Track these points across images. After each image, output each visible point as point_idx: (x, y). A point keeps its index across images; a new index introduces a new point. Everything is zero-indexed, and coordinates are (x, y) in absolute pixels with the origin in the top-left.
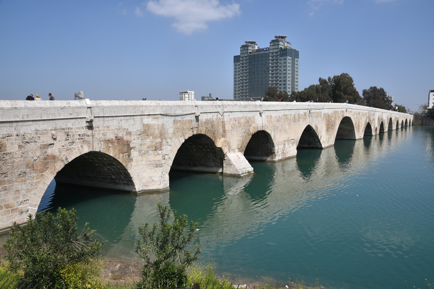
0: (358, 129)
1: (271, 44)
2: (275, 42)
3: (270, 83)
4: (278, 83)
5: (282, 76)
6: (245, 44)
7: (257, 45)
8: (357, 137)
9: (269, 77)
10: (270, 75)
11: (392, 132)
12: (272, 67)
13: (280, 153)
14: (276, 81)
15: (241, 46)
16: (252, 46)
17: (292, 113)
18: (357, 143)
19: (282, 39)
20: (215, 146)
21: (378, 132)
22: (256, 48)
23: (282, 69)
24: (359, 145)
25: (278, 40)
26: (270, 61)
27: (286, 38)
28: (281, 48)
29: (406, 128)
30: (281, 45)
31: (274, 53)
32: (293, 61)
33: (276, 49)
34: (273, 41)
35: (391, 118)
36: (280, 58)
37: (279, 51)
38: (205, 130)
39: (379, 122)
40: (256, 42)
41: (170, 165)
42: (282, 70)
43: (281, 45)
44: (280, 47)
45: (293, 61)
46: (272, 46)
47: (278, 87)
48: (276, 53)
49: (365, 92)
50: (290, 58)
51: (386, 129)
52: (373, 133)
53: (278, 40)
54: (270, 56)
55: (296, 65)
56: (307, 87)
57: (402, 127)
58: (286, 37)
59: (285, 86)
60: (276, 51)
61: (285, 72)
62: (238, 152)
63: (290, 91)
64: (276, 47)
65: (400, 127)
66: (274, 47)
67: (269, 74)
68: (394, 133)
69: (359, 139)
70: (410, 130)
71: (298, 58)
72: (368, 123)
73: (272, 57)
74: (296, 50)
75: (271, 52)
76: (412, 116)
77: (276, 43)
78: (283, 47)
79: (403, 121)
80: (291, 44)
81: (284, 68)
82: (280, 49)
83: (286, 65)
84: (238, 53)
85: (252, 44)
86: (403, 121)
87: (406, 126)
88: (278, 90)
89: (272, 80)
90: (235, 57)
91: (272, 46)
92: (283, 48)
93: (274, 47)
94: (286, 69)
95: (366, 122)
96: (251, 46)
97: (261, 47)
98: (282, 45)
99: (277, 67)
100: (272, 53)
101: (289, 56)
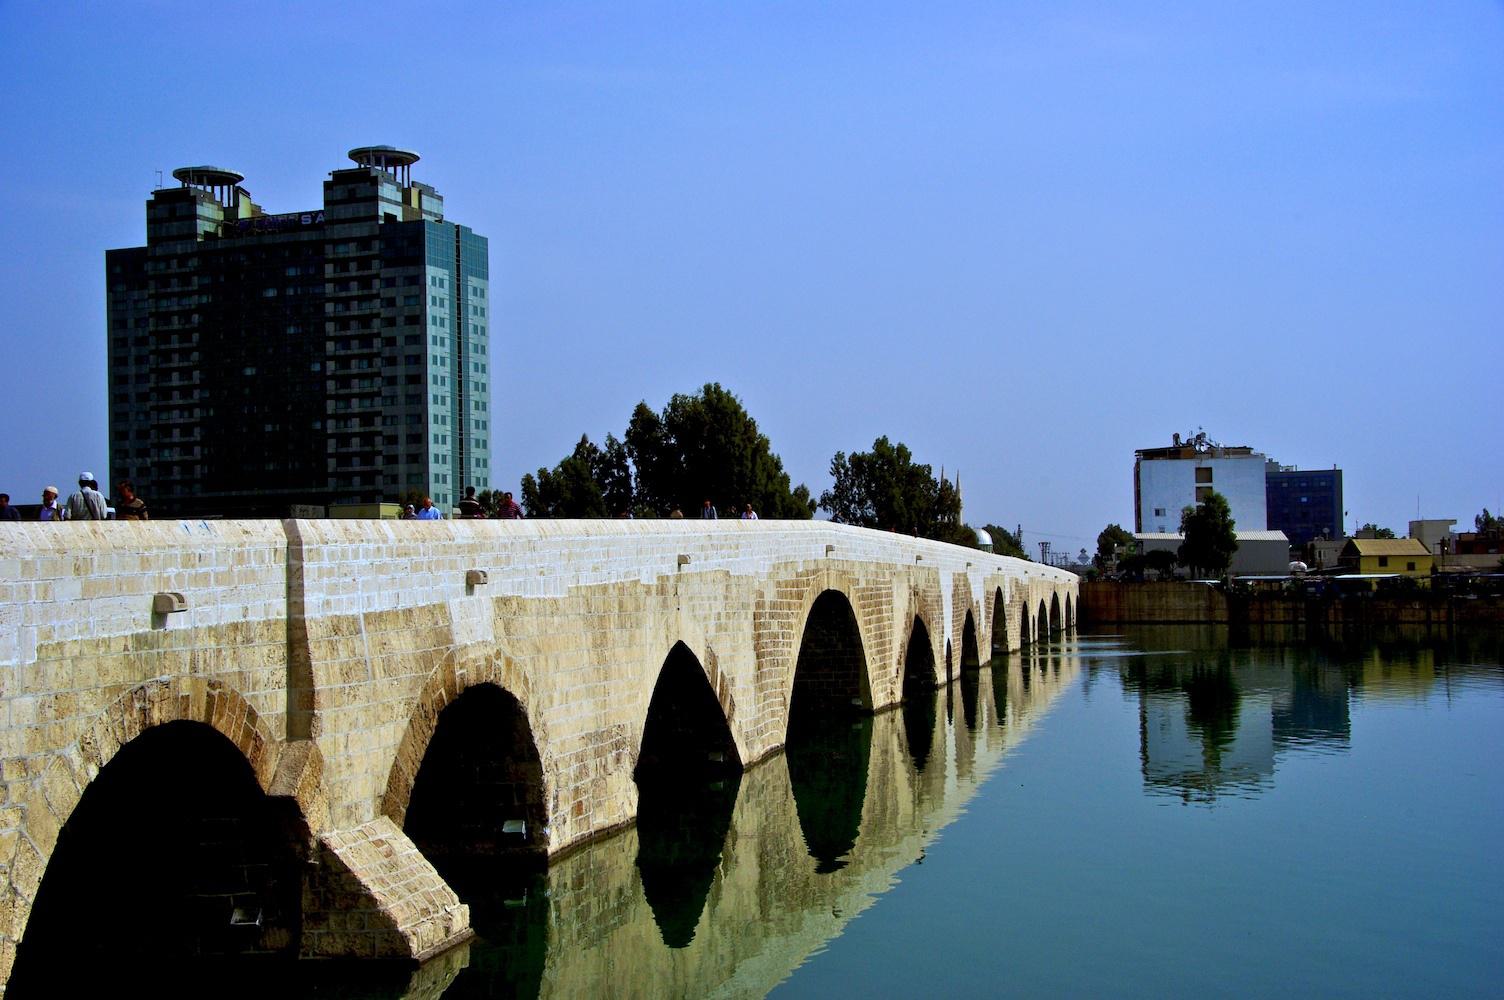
0: (879, 652)
6: (177, 184)
8: (879, 699)
9: (323, 377)
11: (1008, 661)
13: (566, 808)
16: (218, 198)
17: (610, 579)
18: (880, 723)
19: (391, 170)
20: (506, 820)
21: (956, 671)
22: (244, 213)
24: (887, 735)
25: (373, 174)
26: (329, 288)
27: (411, 165)
28: (390, 218)
29: (1056, 639)
30: (388, 201)
34: (340, 177)
35: (999, 594)
36: (387, 273)
37: (377, 232)
38: (205, 698)
39: (956, 615)
40: (241, 179)
41: (15, 938)
42: (400, 340)
43: (388, 201)
49: (915, 464)
51: (985, 654)
52: (941, 677)
53: (373, 174)
55: (475, 313)
56: (628, 425)
57: (1042, 638)
58: (417, 158)
61: (412, 350)
62: (376, 817)
63: (444, 457)
64: (362, 210)
65: (1034, 636)
68: (1014, 665)
69: (883, 710)
70: (1071, 650)
71: (485, 276)
72: (917, 617)
75: (179, 252)
76: (1075, 578)
77: (362, 190)
79: (1042, 604)
80: (440, 198)
81: (409, 330)
82: (381, 222)
84: (137, 237)
85: (399, 169)
86: (1042, 604)
87: (1056, 632)
90: (116, 259)
92: (400, 219)
93: (344, 212)
94: (418, 333)
95: (908, 615)
96: (212, 200)
97: (271, 210)
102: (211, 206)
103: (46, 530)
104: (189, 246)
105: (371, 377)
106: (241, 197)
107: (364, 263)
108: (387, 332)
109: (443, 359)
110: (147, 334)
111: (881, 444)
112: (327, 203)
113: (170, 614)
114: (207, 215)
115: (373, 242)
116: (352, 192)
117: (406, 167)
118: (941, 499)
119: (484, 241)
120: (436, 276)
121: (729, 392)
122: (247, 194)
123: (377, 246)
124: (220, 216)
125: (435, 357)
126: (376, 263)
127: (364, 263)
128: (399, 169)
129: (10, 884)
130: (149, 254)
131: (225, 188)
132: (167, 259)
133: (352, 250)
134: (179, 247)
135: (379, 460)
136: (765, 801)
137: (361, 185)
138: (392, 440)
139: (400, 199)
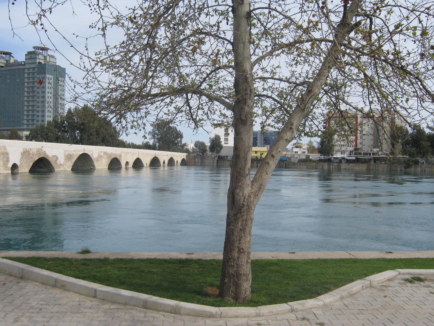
1: (27, 57)
2: (31, 55)
3: (25, 109)
4: (35, 76)
5: (40, 99)
6: (33, 50)
7: (13, 57)
10: (26, 99)
12: (28, 83)
14: (33, 111)
15: (27, 53)
22: (12, 61)
23: (40, 109)
28: (40, 63)
31: (31, 70)
32: (57, 80)
33: (32, 63)
34: (29, 53)
37: (36, 66)
44: (37, 62)
45: (57, 80)
46: (28, 59)
47: (35, 110)
48: (33, 68)
50: (52, 77)
54: (26, 73)
59: (43, 90)
60: (32, 66)
64: (33, 61)
66: (30, 61)
67: (23, 115)
73: (29, 74)
74: (61, 67)
77: (33, 56)
78: (43, 62)
80: (56, 59)
83: (44, 91)
85: (7, 56)
88: (35, 119)
89: (28, 104)
91: (28, 59)
92: (43, 63)
93: (30, 61)
98: (40, 59)
99: (34, 98)
100: (29, 69)
101: (49, 74)
105: (34, 101)
106: (11, 58)
107: (33, 74)
112: (26, 59)
113: (375, 33)
120: (50, 78)
121: (126, 141)
122: (13, 57)
123: (36, 69)
124: (5, 62)
126: (36, 74)
127: (33, 74)
133: (31, 71)
135: (35, 121)
136: (423, 94)
138: (38, 116)
139: (43, 59)
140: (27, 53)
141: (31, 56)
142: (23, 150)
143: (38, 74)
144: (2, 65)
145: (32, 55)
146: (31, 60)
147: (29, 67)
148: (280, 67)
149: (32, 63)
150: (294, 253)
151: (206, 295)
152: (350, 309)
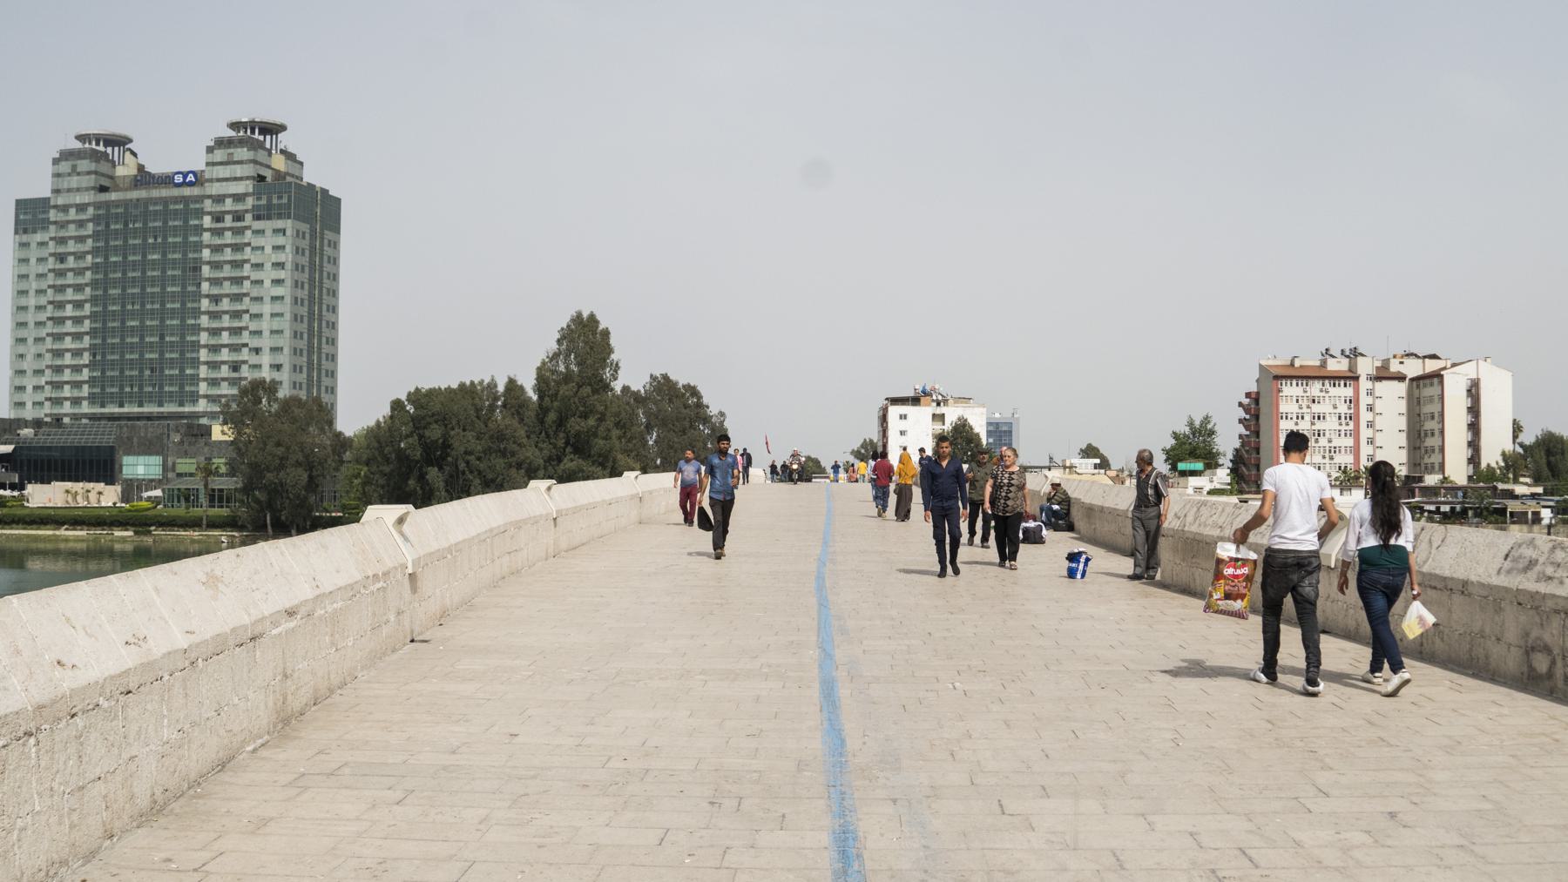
15: (212, 144)
16: (268, 146)
27: (279, 135)
33: (236, 179)
35: (555, 526)
36: (258, 225)
80: (301, 164)
85: (116, 149)
100: (219, 199)
102: (106, 163)
103: (1317, 459)
104: (87, 197)
108: (255, 276)
109: (302, 300)
110: (46, 271)
111: (417, 389)
114: (261, 161)
115: (247, 198)
116: (74, 167)
117: (274, 136)
118: (1549, 453)
119: (338, 201)
122: (134, 154)
125: (302, 305)
126: (248, 217)
127: (238, 217)
128: (268, 137)
129: (272, 819)
130: (52, 203)
131: (116, 149)
132: (64, 209)
133: (229, 205)
134: (78, 198)
137: (239, 150)
140: (212, 144)
141: (231, 154)
142: (959, 419)
143: (258, 218)
144: (103, 183)
145: (231, 150)
146: (228, 167)
147: (221, 192)
148: (942, 574)
149: (236, 179)
150: (188, 632)
151: (1212, 670)
152: (1006, 812)
